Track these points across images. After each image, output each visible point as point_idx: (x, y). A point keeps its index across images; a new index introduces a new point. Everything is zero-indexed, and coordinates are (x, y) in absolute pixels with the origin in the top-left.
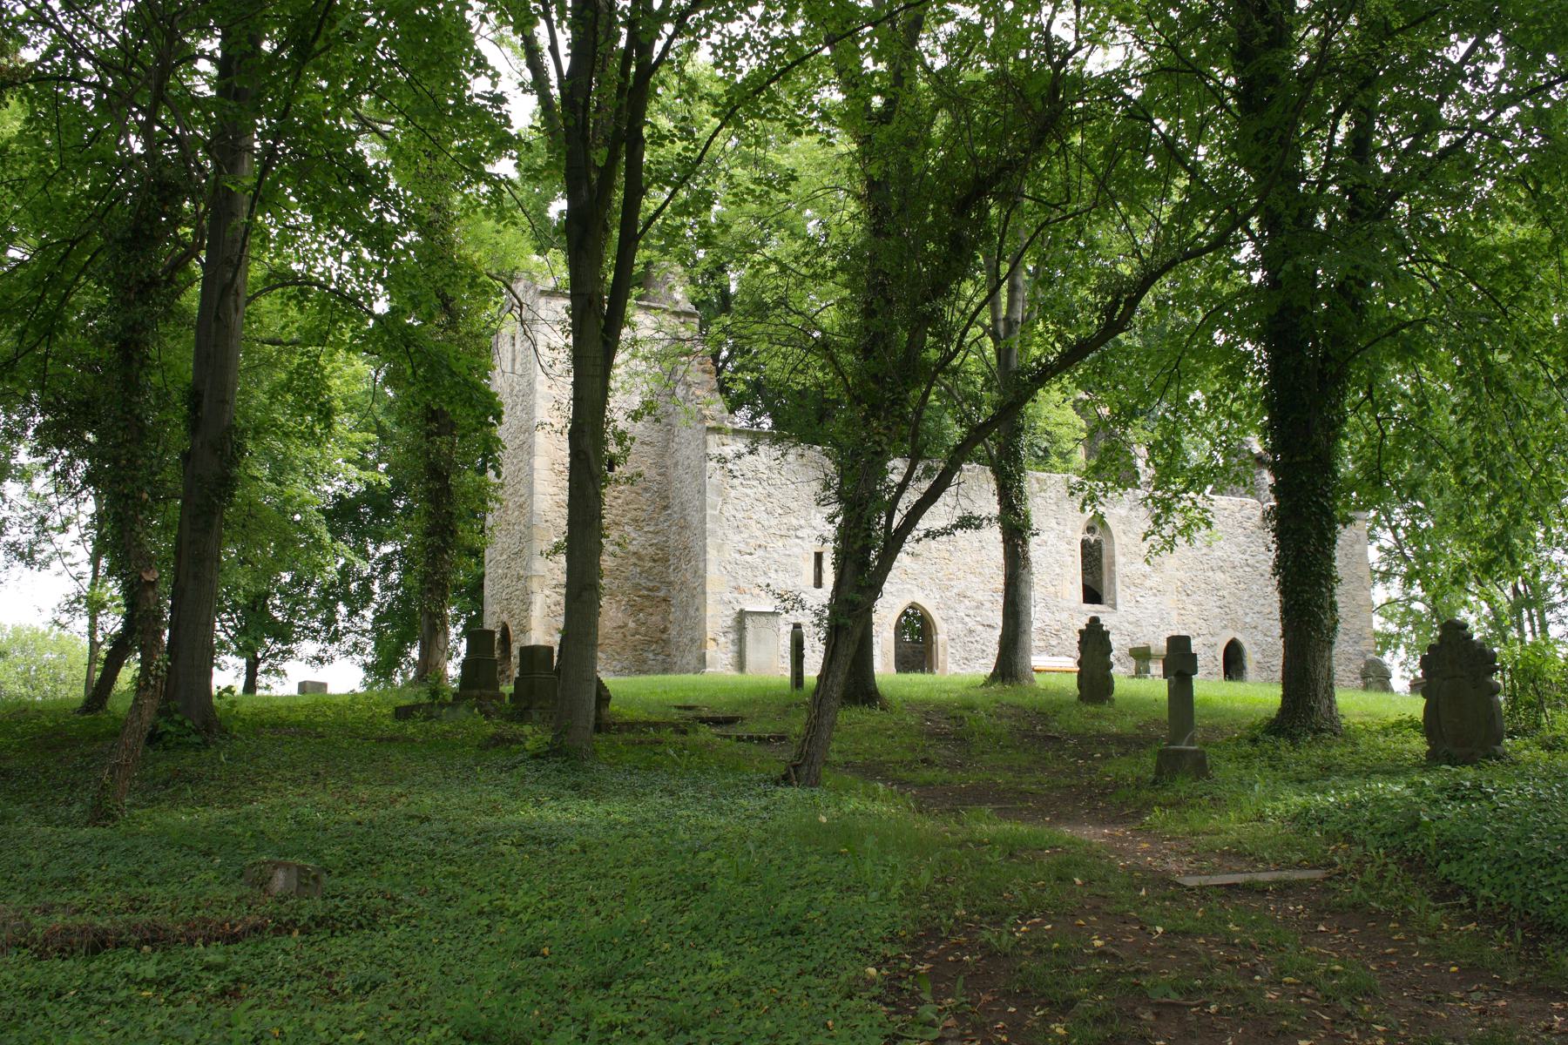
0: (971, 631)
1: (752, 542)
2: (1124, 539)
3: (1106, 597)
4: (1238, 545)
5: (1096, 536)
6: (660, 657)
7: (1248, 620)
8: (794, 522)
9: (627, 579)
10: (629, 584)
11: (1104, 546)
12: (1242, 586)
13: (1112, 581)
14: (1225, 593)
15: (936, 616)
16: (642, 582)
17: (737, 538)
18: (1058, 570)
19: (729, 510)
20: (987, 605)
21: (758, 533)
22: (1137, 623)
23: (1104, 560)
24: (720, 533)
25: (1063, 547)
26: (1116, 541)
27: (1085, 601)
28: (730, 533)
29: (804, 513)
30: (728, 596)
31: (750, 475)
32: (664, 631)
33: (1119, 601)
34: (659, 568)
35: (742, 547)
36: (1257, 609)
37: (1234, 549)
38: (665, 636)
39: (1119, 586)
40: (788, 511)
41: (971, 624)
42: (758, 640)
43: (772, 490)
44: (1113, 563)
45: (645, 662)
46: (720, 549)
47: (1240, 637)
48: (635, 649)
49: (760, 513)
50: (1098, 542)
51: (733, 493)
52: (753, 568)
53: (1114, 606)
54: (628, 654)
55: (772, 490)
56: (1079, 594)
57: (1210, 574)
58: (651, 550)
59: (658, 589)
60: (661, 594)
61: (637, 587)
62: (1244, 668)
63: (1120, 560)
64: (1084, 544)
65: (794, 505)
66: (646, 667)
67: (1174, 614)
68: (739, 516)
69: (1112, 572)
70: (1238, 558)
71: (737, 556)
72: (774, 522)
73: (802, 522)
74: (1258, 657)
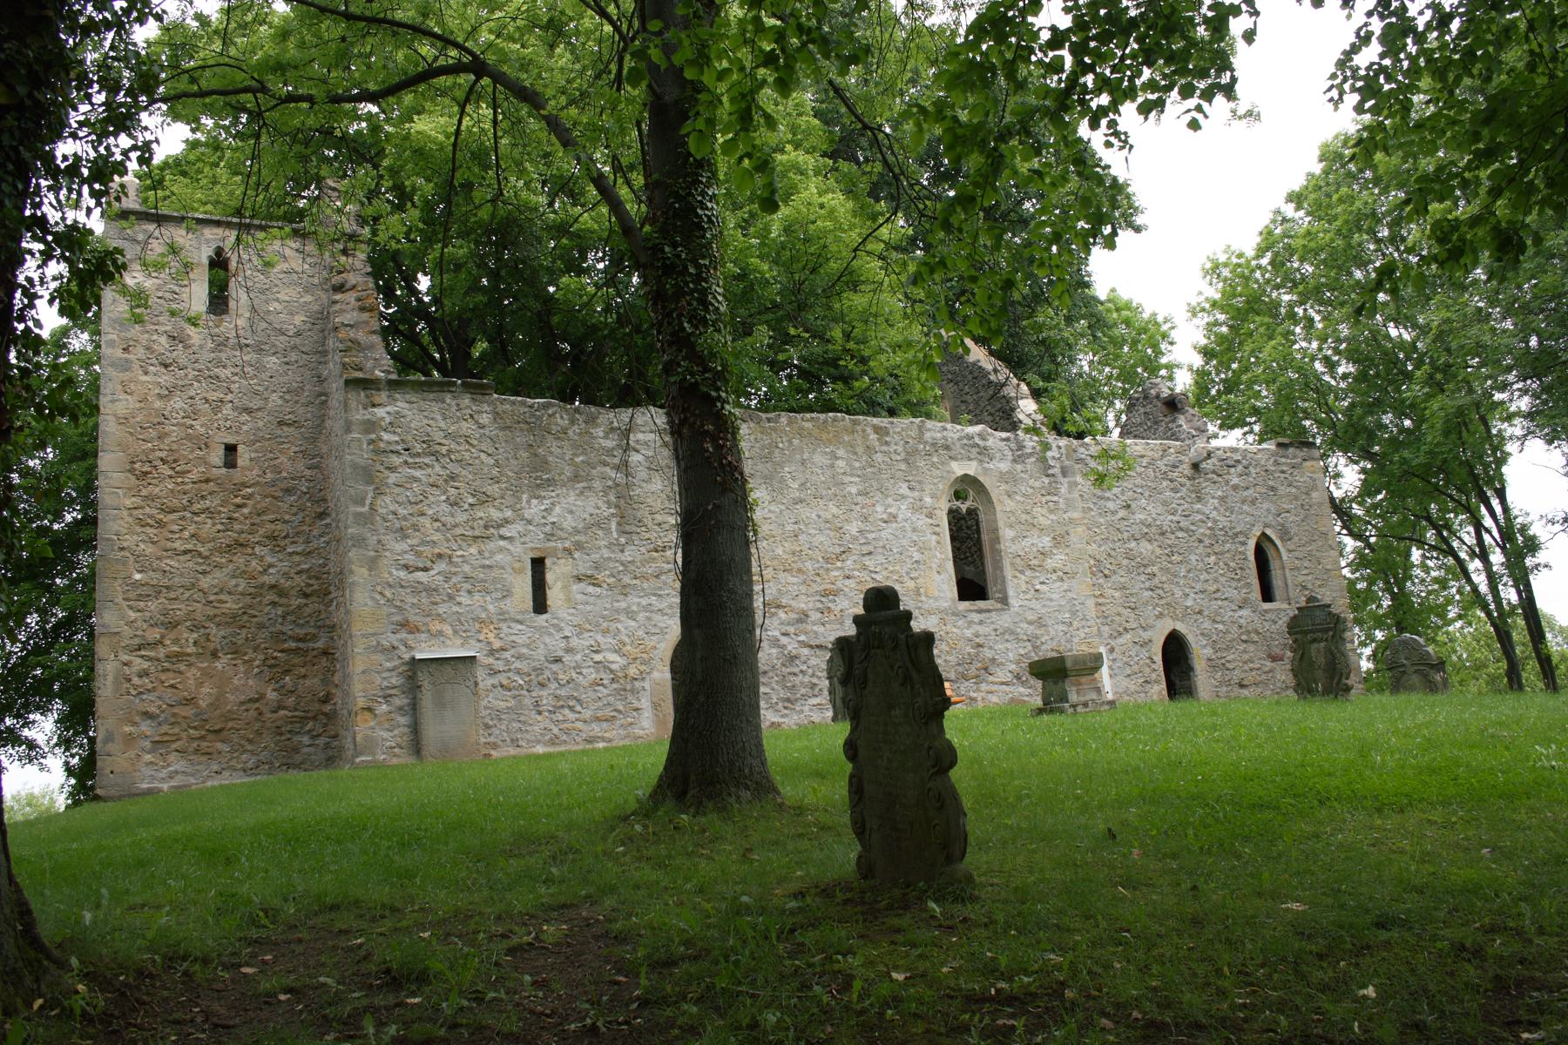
0: (793, 658)
1: (428, 551)
2: (1010, 505)
3: (992, 589)
4: (1165, 503)
5: (968, 504)
6: (321, 741)
7: (1189, 603)
8: (495, 515)
9: (261, 626)
10: (264, 634)
11: (982, 517)
12: (1176, 558)
13: (998, 566)
14: (1155, 569)
15: (1190, 638)
16: (287, 628)
17: (400, 547)
18: (917, 556)
19: (386, 504)
20: (815, 616)
21: (437, 537)
22: (1039, 622)
23: (985, 537)
24: (372, 540)
25: (922, 521)
26: (998, 508)
27: (963, 596)
28: (388, 539)
29: (509, 500)
30: (389, 639)
31: (418, 448)
32: (326, 699)
33: (1011, 593)
34: (314, 605)
35: (410, 558)
36: (1198, 587)
37: (1160, 509)
38: (327, 708)
39: (1008, 572)
40: (484, 500)
41: (791, 646)
42: (440, 704)
43: (457, 469)
44: (997, 540)
45: (296, 750)
46: (372, 565)
47: (1181, 627)
48: (278, 731)
49: (438, 504)
50: (972, 513)
51: (393, 478)
52: (431, 590)
53: (1004, 600)
54: (268, 740)
55: (457, 469)
56: (953, 591)
57: (1133, 544)
58: (299, 581)
59: (314, 638)
60: (320, 644)
61: (278, 637)
62: (1191, 669)
63: (1007, 533)
64: (954, 515)
65: (493, 489)
66: (298, 758)
67: (1091, 603)
68: (402, 511)
69: (997, 553)
70: (1166, 520)
71: (402, 574)
72: (461, 517)
73: (509, 514)
74: (1208, 651)
